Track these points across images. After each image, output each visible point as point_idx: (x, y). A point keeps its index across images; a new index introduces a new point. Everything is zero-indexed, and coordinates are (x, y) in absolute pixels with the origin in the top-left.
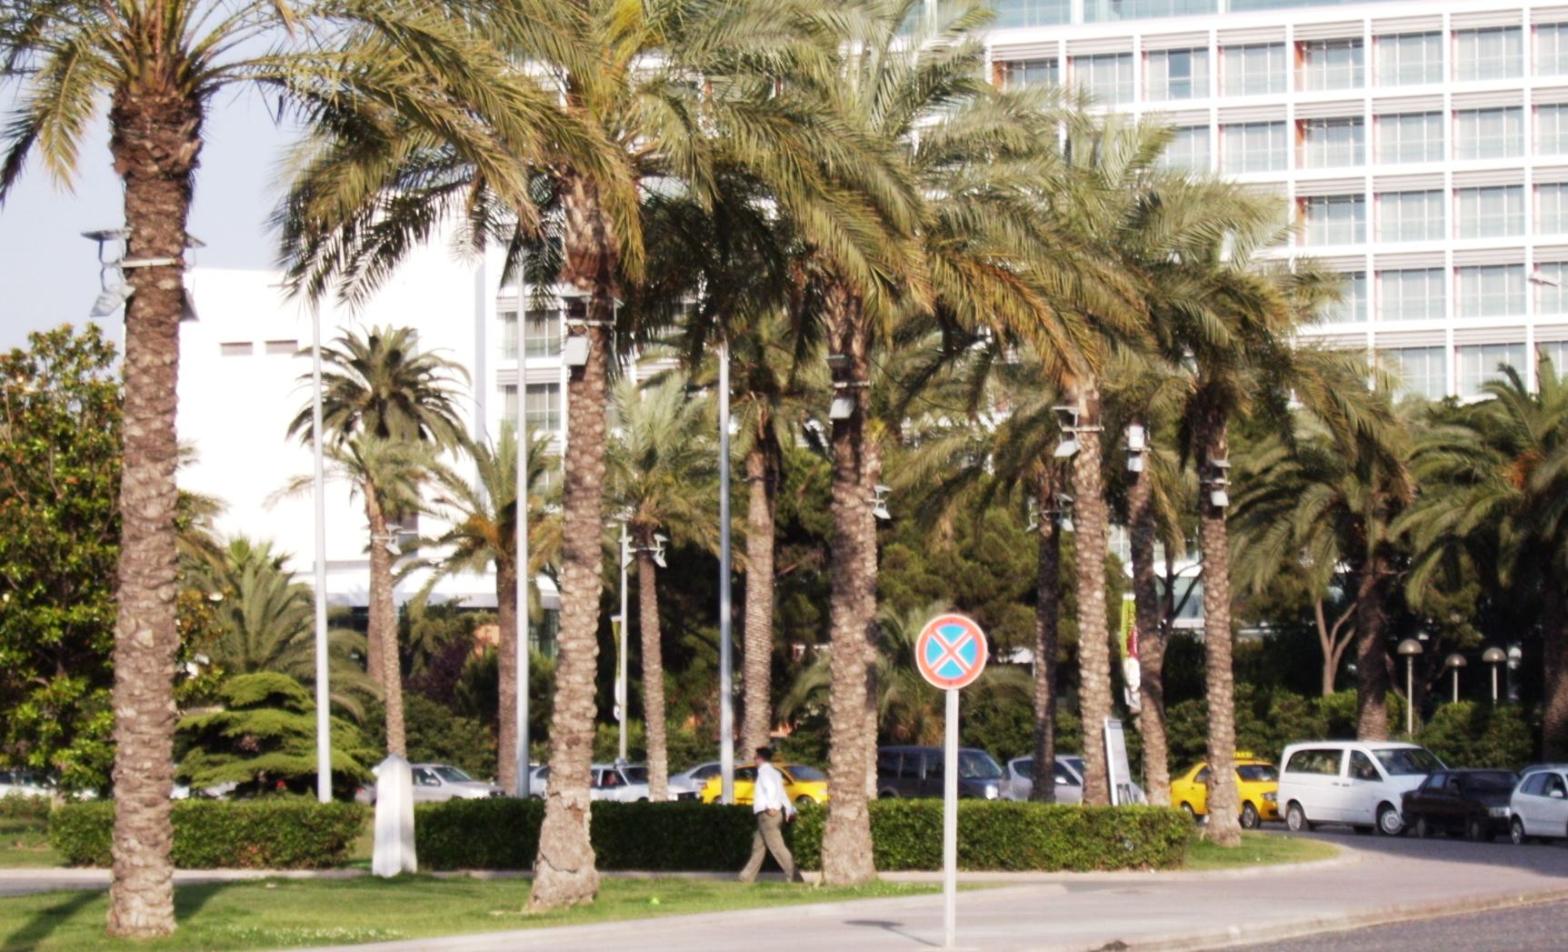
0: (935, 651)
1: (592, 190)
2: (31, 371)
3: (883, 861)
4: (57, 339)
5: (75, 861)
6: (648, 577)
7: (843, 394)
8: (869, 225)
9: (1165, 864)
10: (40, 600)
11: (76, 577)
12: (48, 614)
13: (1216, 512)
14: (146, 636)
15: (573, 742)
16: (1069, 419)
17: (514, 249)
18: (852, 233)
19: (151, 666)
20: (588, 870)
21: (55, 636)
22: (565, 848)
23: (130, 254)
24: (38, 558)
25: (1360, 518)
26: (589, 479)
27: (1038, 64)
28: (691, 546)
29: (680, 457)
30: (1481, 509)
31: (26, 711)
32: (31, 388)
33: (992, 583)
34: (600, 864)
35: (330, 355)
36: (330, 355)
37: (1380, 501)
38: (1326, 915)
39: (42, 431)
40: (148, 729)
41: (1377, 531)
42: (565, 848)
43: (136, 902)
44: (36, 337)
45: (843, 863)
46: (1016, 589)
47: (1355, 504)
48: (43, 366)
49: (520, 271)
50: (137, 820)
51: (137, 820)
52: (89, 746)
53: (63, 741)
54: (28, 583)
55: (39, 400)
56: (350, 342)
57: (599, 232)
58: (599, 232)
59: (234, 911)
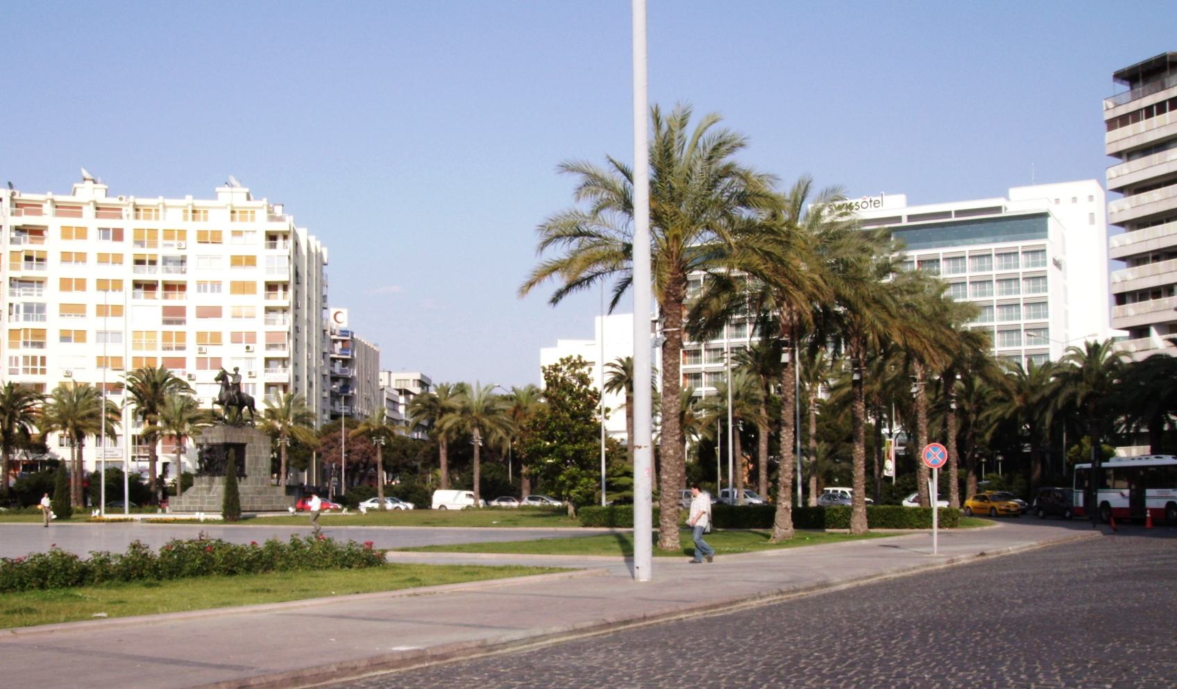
0: (929, 455)
1: (790, 305)
2: (560, 370)
3: (871, 525)
4: (568, 360)
5: (586, 525)
6: (737, 434)
7: (857, 372)
8: (884, 316)
9: (951, 526)
10: (565, 442)
11: (576, 436)
12: (567, 447)
13: (952, 410)
14: (671, 452)
15: (785, 487)
16: (915, 380)
17: (756, 324)
18: (880, 319)
19: (672, 461)
20: (791, 529)
21: (571, 454)
22: (783, 522)
23: (665, 327)
24: (564, 428)
25: (968, 413)
26: (790, 400)
27: (931, 261)
28: (751, 424)
29: (746, 397)
30: (1011, 410)
31: (562, 478)
32: (561, 375)
33: (835, 435)
34: (795, 527)
35: (614, 366)
36: (614, 366)
37: (974, 407)
38: (1033, 543)
39: (564, 389)
40: (671, 483)
41: (973, 418)
42: (783, 522)
43: (668, 539)
44: (562, 360)
45: (858, 526)
46: (844, 437)
47: (967, 408)
48: (565, 368)
49: (757, 332)
50: (668, 512)
51: (668, 512)
52: (581, 489)
53: (572, 487)
54: (562, 437)
55: (563, 379)
56: (621, 361)
57: (792, 319)
58: (792, 319)
59: (1073, 561)
